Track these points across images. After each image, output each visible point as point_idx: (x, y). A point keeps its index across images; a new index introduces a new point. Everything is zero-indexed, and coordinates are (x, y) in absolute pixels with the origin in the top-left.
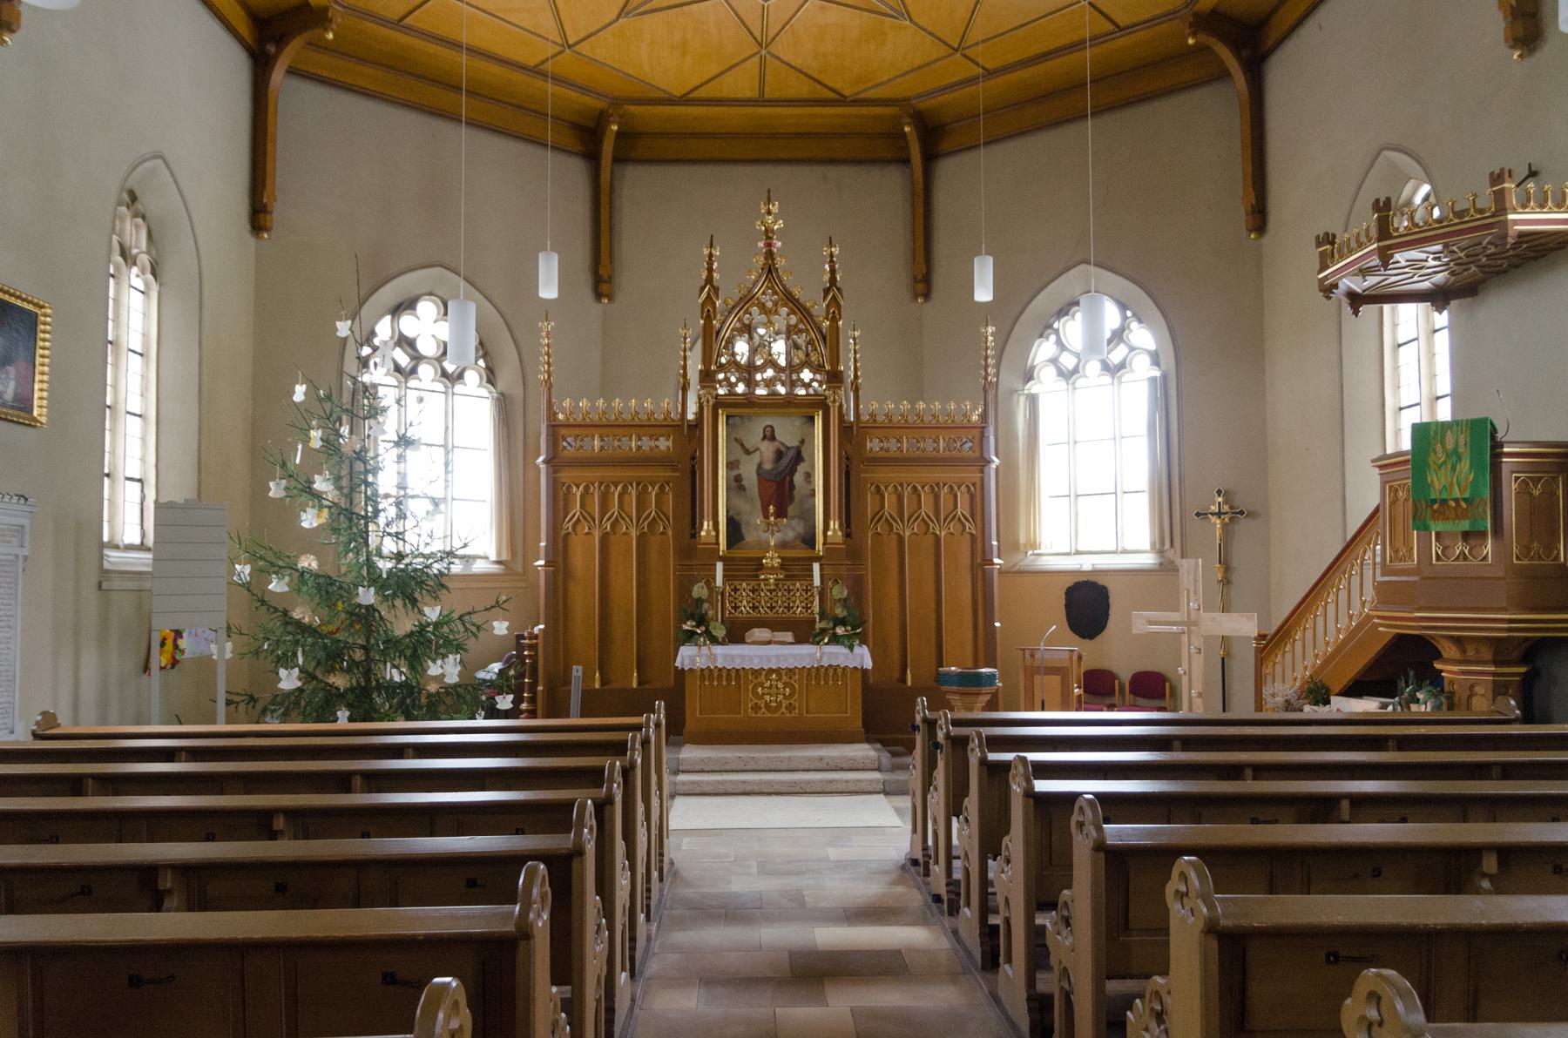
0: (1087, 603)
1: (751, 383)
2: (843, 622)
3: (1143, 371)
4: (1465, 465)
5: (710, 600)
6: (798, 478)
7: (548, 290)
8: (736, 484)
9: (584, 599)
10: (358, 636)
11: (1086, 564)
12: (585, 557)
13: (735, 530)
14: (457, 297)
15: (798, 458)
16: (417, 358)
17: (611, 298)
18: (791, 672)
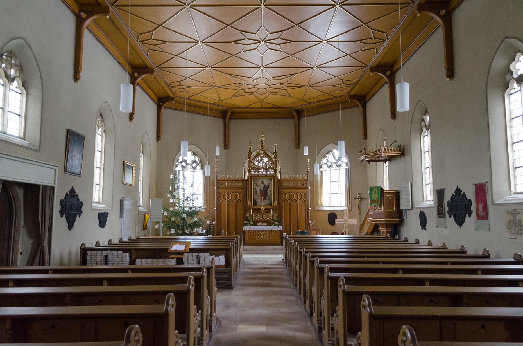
0: (332, 217)
1: (259, 172)
2: (277, 221)
3: (344, 166)
4: (377, 194)
5: (250, 217)
6: (268, 191)
7: (218, 154)
8: (255, 193)
9: (224, 216)
10: (181, 222)
11: (332, 209)
12: (224, 207)
13: (255, 203)
14: (183, 140)
15: (268, 187)
16: (187, 164)
17: (228, 149)
18: (266, 231)
